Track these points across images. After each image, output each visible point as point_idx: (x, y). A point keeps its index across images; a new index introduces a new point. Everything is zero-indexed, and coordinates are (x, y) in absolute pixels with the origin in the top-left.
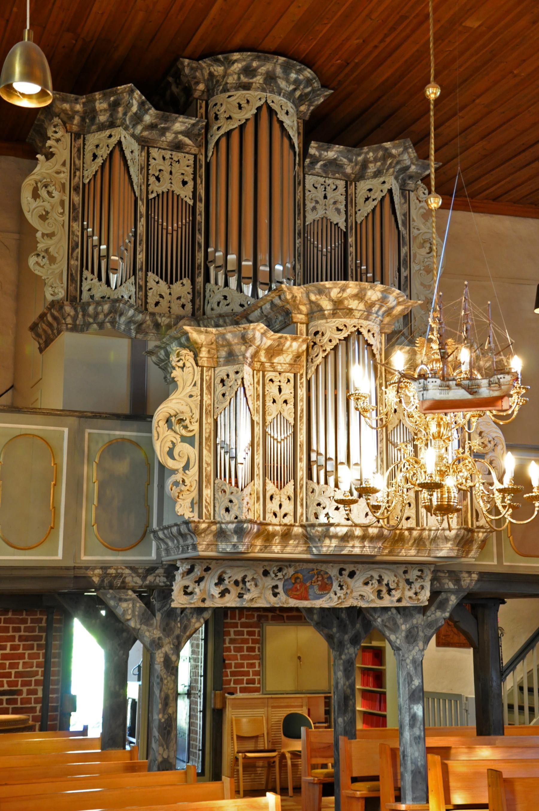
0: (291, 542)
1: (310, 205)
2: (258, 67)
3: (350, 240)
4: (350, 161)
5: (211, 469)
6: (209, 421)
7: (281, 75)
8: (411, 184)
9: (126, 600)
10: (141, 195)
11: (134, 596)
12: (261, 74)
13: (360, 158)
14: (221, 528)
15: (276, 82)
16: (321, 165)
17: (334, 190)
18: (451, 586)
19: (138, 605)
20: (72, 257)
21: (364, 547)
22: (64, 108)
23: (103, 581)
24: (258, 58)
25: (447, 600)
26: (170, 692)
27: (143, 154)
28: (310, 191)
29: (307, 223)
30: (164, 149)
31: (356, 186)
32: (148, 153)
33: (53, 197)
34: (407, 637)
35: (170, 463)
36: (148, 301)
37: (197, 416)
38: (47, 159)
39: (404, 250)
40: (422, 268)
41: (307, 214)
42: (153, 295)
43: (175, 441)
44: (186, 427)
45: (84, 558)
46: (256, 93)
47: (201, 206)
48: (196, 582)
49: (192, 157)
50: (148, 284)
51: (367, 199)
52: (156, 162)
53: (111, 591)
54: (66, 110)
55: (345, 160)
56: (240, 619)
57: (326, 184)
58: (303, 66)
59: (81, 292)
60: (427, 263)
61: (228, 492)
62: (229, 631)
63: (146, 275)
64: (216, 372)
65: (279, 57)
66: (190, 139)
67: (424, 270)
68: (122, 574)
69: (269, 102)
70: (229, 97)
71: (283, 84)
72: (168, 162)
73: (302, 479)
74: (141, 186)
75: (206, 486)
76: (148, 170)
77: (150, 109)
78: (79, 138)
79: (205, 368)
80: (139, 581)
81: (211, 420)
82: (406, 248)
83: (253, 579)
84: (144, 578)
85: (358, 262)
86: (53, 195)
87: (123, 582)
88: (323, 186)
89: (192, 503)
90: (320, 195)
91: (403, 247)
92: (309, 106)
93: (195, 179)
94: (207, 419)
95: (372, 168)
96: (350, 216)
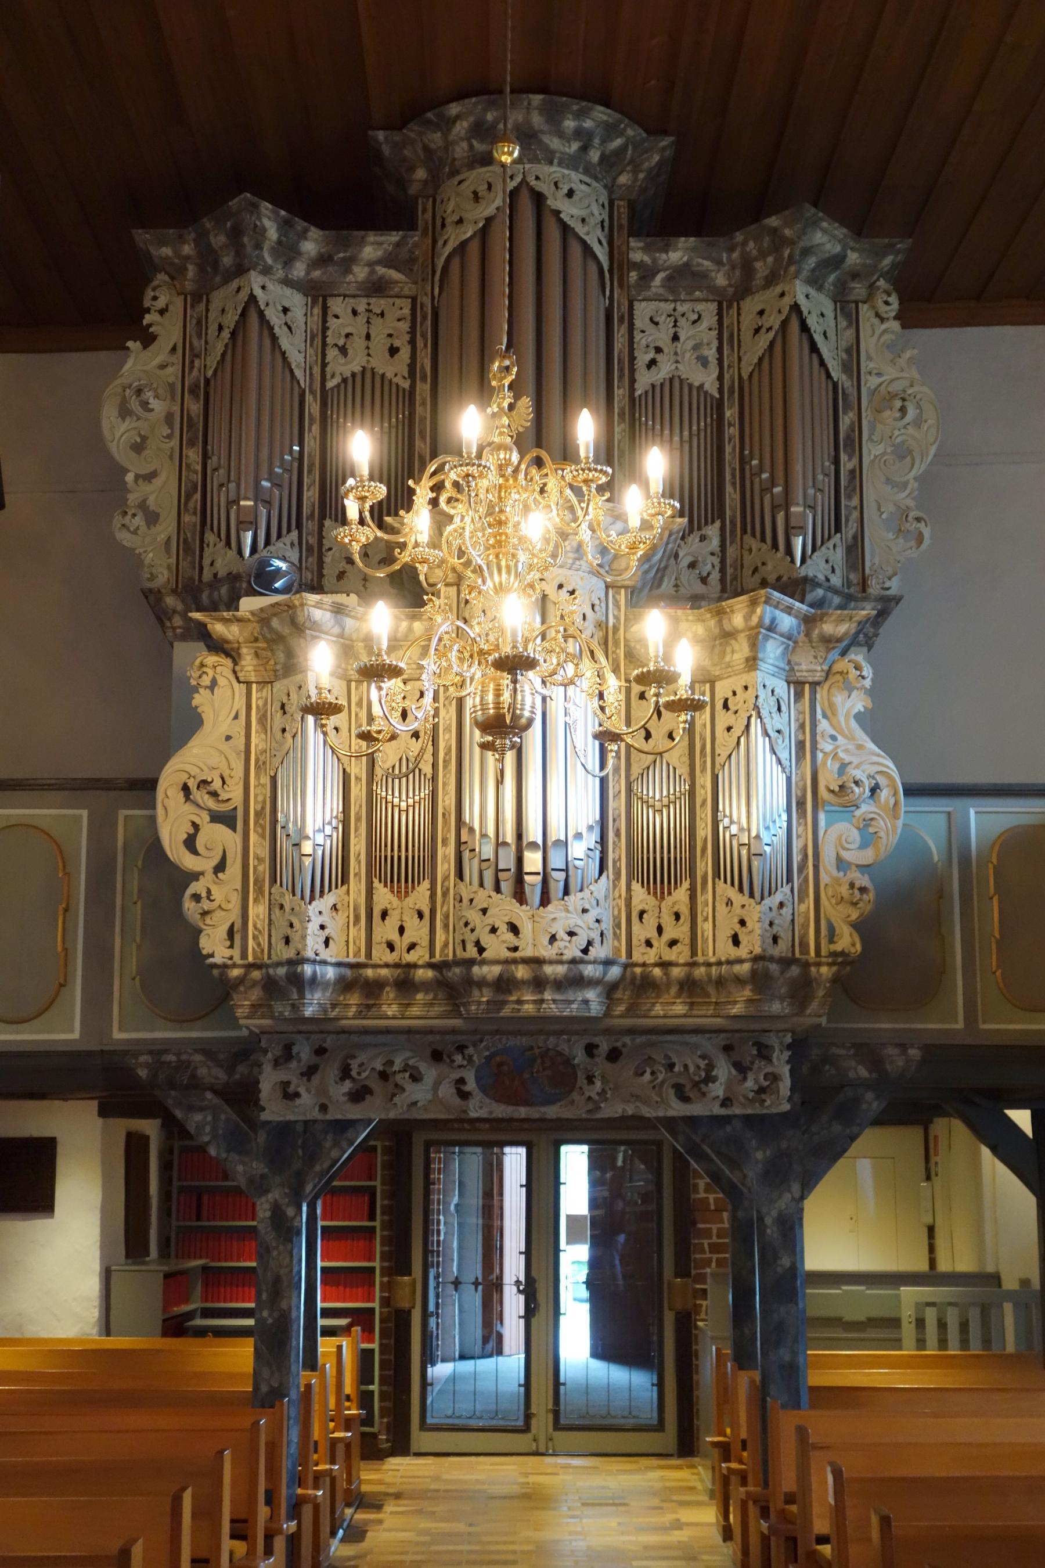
0: (420, 996)
1: (643, 358)
3: (728, 414)
4: (719, 263)
5: (265, 868)
6: (262, 781)
7: (546, 127)
8: (858, 289)
9: (201, 1109)
11: (216, 1101)
13: (735, 255)
14: (268, 974)
15: (540, 142)
16: (663, 280)
17: (694, 322)
18: (863, 1072)
19: (223, 1117)
20: (186, 510)
21: (542, 1001)
22: (164, 255)
25: (857, 1101)
26: (283, 1271)
27: (316, 311)
28: (643, 332)
29: (637, 393)
30: (354, 296)
31: (739, 309)
32: (325, 309)
33: (153, 410)
35: (188, 862)
36: (325, 572)
37: (239, 772)
38: (145, 346)
39: (846, 421)
40: (889, 450)
41: (637, 376)
42: (333, 560)
43: (198, 821)
44: (214, 794)
45: (117, 1035)
48: (302, 1074)
50: (325, 541)
51: (757, 331)
53: (173, 1093)
54: (168, 257)
55: (706, 263)
58: (584, 104)
59: (201, 568)
60: (899, 440)
61: (287, 908)
63: (321, 526)
64: (275, 690)
65: (531, 96)
66: (399, 271)
67: (892, 452)
68: (189, 1062)
70: (460, 182)
71: (555, 143)
72: (362, 319)
73: (446, 878)
74: (311, 368)
75: (256, 900)
76: (324, 337)
77: (306, 231)
78: (200, 301)
79: (254, 686)
80: (221, 1075)
81: (266, 780)
82: (851, 414)
83: (406, 1068)
84: (230, 1070)
85: (747, 452)
86: (150, 406)
87: (193, 1076)
89: (231, 933)
90: (662, 336)
91: (845, 413)
92: (635, 172)
93: (412, 342)
94: (257, 776)
95: (762, 268)
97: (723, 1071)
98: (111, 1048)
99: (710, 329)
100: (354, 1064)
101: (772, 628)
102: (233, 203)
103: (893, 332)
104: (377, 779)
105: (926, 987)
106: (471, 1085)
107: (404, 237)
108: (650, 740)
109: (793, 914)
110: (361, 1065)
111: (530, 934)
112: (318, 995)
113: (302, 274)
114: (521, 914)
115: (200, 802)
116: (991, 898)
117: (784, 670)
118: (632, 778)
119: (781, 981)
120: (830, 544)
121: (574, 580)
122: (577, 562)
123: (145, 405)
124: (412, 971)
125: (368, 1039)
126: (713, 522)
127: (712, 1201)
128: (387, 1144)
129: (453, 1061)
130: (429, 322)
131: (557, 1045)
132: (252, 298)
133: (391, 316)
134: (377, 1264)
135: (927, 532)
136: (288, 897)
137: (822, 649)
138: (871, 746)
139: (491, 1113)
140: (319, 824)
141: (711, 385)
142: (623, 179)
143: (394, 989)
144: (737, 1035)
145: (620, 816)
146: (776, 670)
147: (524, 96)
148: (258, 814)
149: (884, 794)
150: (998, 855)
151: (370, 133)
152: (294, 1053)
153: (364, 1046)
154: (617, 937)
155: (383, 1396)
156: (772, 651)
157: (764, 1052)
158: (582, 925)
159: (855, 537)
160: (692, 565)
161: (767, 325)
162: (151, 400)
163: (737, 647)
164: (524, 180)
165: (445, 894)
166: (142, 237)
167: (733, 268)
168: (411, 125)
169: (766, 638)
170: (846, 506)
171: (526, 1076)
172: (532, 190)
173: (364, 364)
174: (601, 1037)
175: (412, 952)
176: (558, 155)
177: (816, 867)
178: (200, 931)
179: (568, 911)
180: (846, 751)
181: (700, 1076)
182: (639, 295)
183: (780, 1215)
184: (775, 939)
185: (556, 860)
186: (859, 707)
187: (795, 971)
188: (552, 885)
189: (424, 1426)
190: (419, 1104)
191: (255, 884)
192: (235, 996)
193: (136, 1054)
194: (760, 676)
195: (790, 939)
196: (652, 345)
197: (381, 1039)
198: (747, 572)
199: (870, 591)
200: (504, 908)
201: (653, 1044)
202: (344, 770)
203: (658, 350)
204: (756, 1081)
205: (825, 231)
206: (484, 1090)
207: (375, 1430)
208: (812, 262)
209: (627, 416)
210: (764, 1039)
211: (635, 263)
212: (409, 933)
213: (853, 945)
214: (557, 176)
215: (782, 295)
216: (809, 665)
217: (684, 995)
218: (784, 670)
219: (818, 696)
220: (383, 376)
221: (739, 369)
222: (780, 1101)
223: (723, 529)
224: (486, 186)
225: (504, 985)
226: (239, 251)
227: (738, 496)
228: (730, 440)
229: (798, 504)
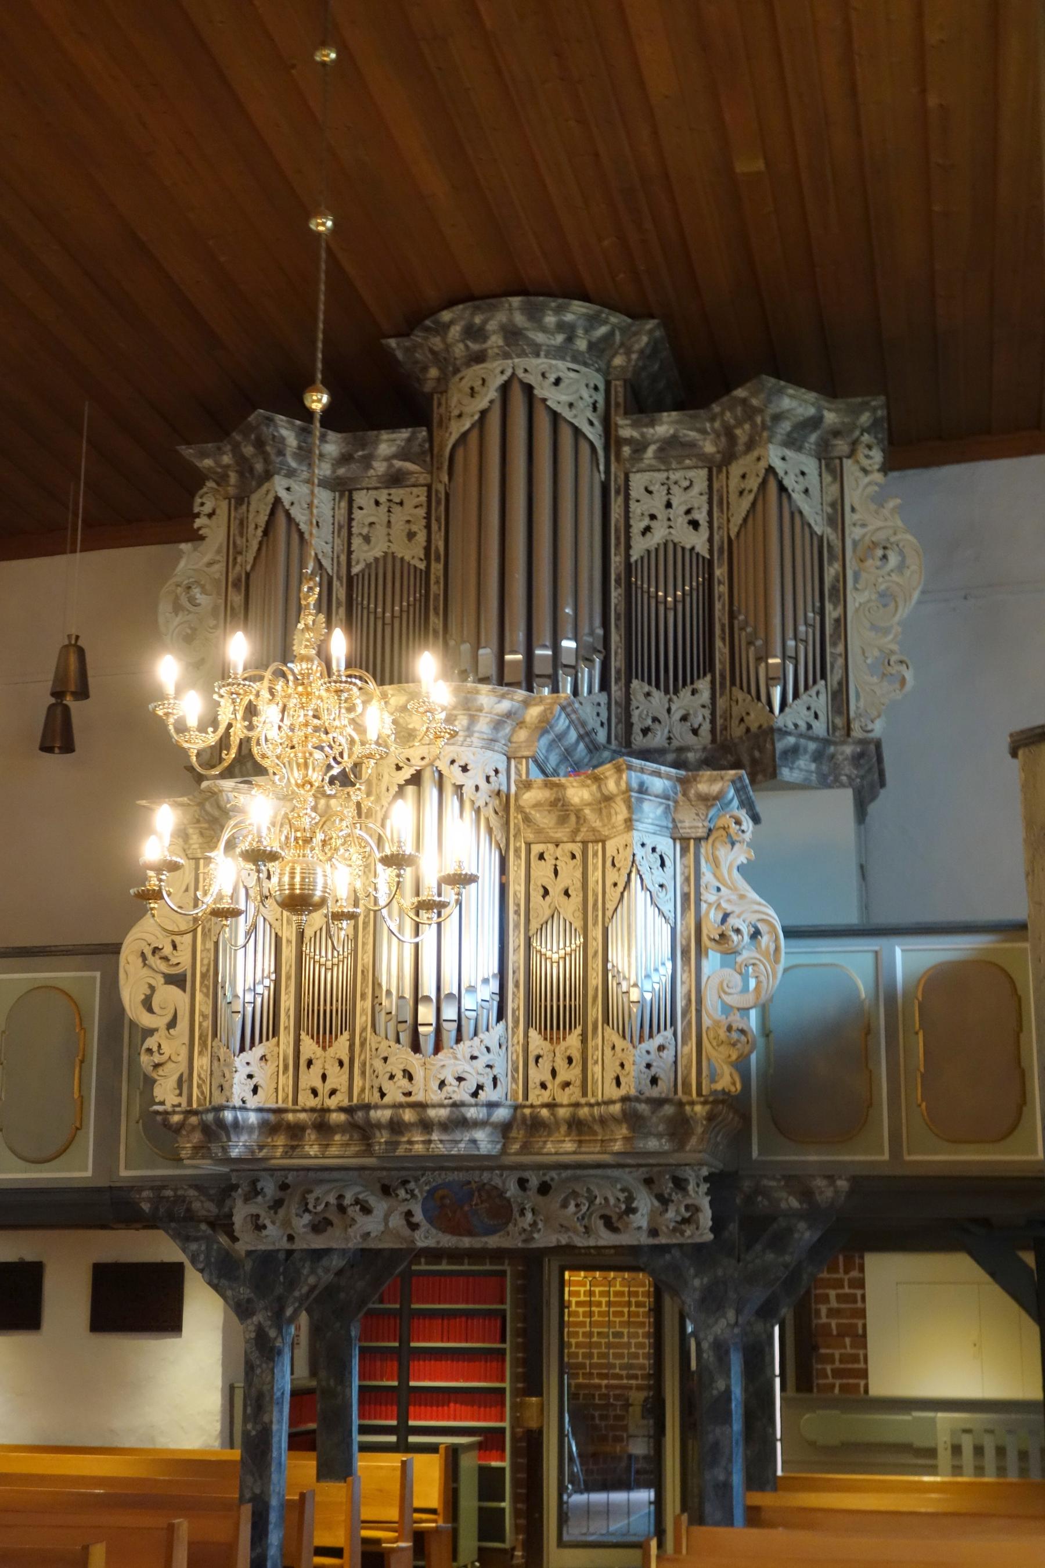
0: (337, 1137)
1: (637, 526)
2: (485, 322)
4: (703, 432)
5: (208, 1024)
7: (527, 325)
8: (841, 446)
9: (196, 1239)
10: (338, 571)
12: (494, 332)
15: (527, 338)
17: (686, 489)
18: (794, 1203)
21: (430, 1142)
23: (157, 1208)
24: (478, 308)
25: (790, 1230)
26: (266, 1388)
29: (633, 560)
30: (376, 488)
31: (728, 472)
32: (351, 501)
33: (199, 605)
34: (703, 1300)
35: (146, 1020)
39: (831, 571)
41: (633, 543)
43: (153, 983)
44: (166, 959)
45: (124, 1173)
46: (496, 364)
47: (437, 568)
48: (270, 1208)
49: (423, 492)
52: (364, 511)
56: (846, 1272)
57: (670, 482)
58: (560, 301)
62: (827, 1295)
65: (510, 299)
66: (414, 463)
68: (185, 1197)
69: (521, 374)
70: (461, 379)
71: (540, 338)
72: (383, 509)
74: (338, 557)
75: (200, 1053)
76: (350, 527)
81: (210, 945)
83: (357, 1202)
87: (189, 1210)
88: (666, 487)
89: (180, 1082)
90: (656, 504)
91: (830, 563)
92: (628, 352)
93: (428, 527)
94: (203, 942)
95: (742, 434)
96: (719, 528)
97: (645, 1203)
98: (118, 1184)
99: (701, 494)
100: (311, 1199)
101: (642, 790)
102: (252, 418)
103: (876, 484)
104: (306, 940)
105: (852, 1121)
106: (419, 1217)
107: (413, 434)
108: (547, 898)
109: (676, 1056)
110: (317, 1199)
111: (422, 1080)
112: (244, 1138)
113: (328, 473)
114: (414, 1061)
115: (154, 966)
116: (917, 1033)
117: (667, 828)
118: (531, 933)
119: (654, 1119)
120: (813, 692)
121: (465, 755)
122: (468, 739)
123: (192, 601)
124: (327, 1115)
125: (326, 1175)
126: (705, 675)
127: (834, 1326)
128: (520, 1268)
129: (397, 1195)
130: (442, 508)
131: (491, 1179)
132: (278, 500)
133: (410, 503)
134: (507, 1385)
135: (909, 675)
136: (223, 1050)
137: (702, 807)
138: (753, 895)
139: (438, 1242)
140: (250, 983)
141: (702, 549)
142: (618, 361)
143: (314, 1131)
144: (655, 1169)
145: (519, 968)
146: (658, 828)
147: (504, 299)
148: (204, 976)
149: (765, 940)
150: (923, 991)
151: (384, 341)
152: (259, 1188)
153: (321, 1182)
154: (515, 1080)
155: (517, 1514)
156: (651, 811)
157: (680, 1184)
158: (476, 1073)
159: (840, 683)
160: (684, 718)
161: (748, 488)
162: (198, 596)
163: (618, 810)
164: (513, 374)
165: (363, 1044)
166: (187, 452)
167: (718, 436)
168: (416, 332)
169: (640, 801)
170: (832, 653)
171: (466, 1208)
172: (521, 382)
173: (385, 550)
174: (531, 1172)
175: (333, 1097)
176: (544, 348)
177: (699, 1011)
178: (155, 1081)
179: (456, 1058)
180: (729, 901)
181: (620, 1208)
182: (633, 466)
183: (716, 1339)
184: (654, 1081)
185: (449, 1012)
186: (742, 859)
187: (668, 1110)
188: (445, 1035)
189: (561, 1544)
190: (373, 1235)
191: (200, 1038)
192: (179, 1139)
193: (141, 1189)
194: (636, 837)
195: (672, 1079)
196: (646, 513)
197: (336, 1175)
198: (735, 722)
199: (854, 734)
200: (402, 1056)
201: (577, 1179)
202: (276, 934)
203: (653, 517)
204: (677, 1212)
205: (791, 397)
206: (430, 1221)
207: (507, 1545)
208: (786, 426)
209: (623, 581)
210: (680, 1173)
211: (626, 440)
212: (330, 1078)
213: (734, 1084)
214: (543, 367)
215: (759, 459)
216: (692, 823)
217: (574, 1133)
218: (667, 828)
219: (703, 850)
220: (402, 559)
221: (728, 529)
222: (703, 1231)
223: (713, 682)
224: (480, 382)
225: (396, 1127)
226: (267, 460)
227: (727, 651)
228: (720, 597)
229: (775, 656)
